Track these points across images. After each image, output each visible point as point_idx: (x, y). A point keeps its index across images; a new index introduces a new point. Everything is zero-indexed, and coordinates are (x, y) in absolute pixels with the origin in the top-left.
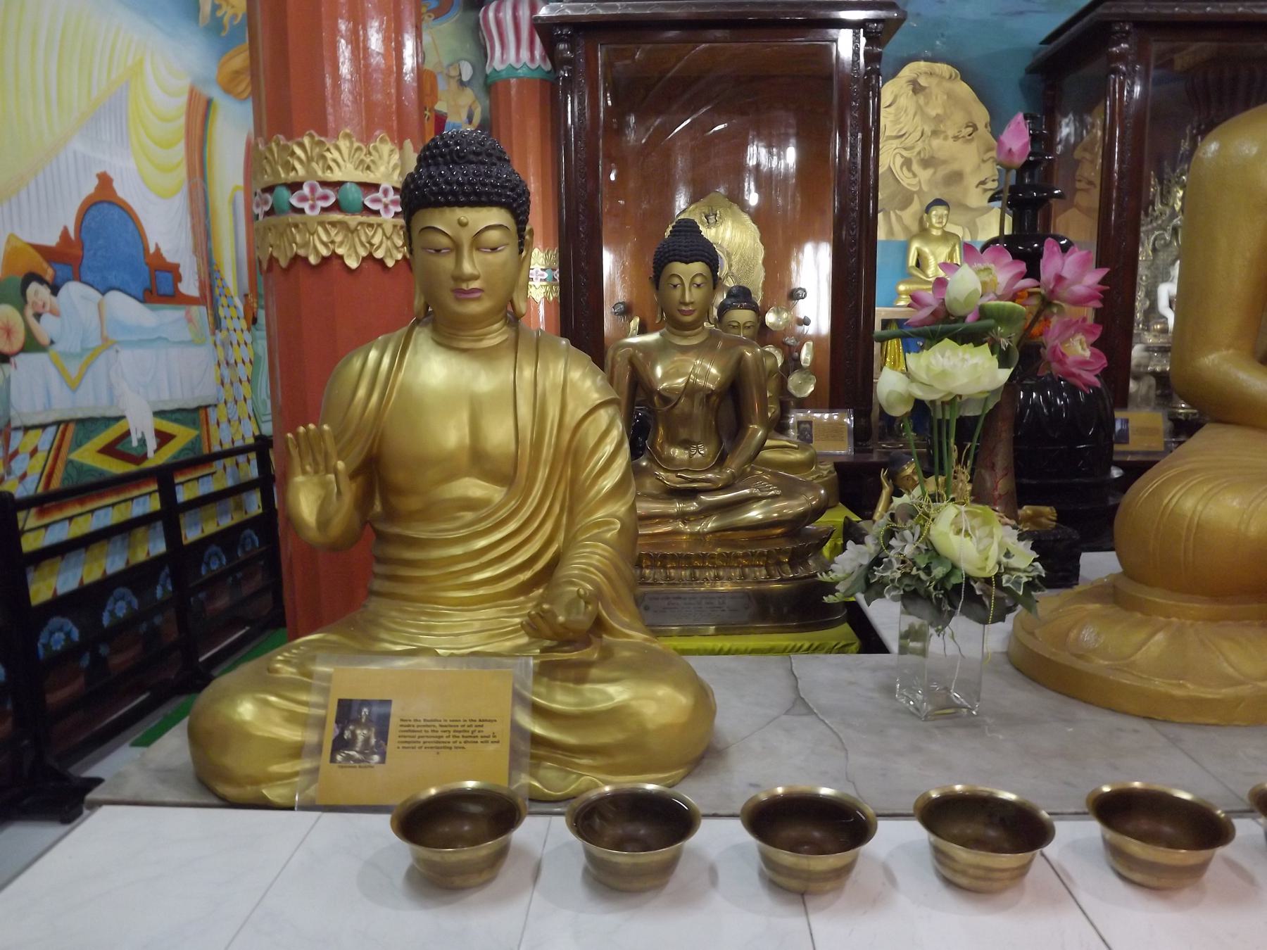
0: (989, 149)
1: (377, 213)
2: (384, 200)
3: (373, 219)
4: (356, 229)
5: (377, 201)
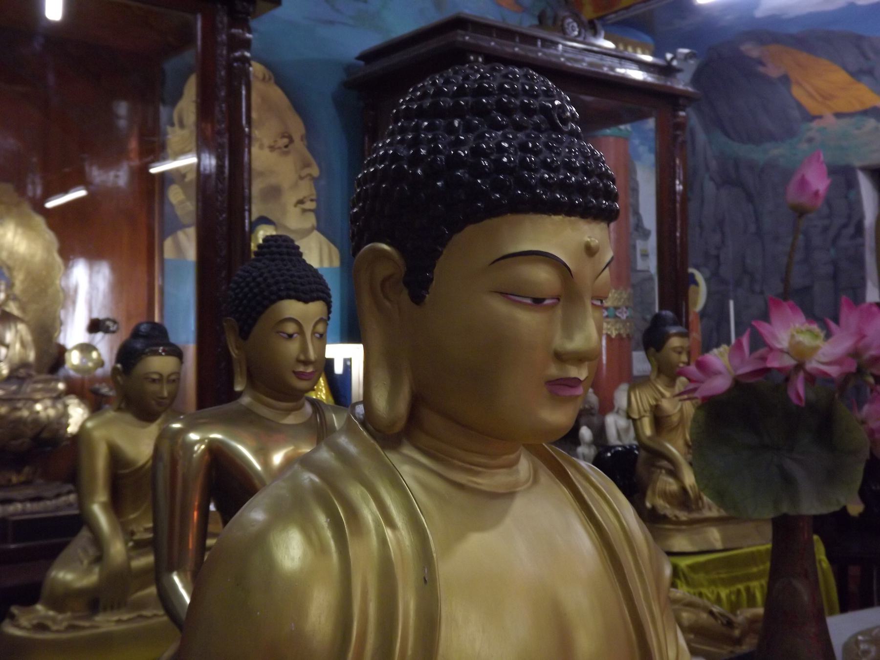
0: (307, 165)
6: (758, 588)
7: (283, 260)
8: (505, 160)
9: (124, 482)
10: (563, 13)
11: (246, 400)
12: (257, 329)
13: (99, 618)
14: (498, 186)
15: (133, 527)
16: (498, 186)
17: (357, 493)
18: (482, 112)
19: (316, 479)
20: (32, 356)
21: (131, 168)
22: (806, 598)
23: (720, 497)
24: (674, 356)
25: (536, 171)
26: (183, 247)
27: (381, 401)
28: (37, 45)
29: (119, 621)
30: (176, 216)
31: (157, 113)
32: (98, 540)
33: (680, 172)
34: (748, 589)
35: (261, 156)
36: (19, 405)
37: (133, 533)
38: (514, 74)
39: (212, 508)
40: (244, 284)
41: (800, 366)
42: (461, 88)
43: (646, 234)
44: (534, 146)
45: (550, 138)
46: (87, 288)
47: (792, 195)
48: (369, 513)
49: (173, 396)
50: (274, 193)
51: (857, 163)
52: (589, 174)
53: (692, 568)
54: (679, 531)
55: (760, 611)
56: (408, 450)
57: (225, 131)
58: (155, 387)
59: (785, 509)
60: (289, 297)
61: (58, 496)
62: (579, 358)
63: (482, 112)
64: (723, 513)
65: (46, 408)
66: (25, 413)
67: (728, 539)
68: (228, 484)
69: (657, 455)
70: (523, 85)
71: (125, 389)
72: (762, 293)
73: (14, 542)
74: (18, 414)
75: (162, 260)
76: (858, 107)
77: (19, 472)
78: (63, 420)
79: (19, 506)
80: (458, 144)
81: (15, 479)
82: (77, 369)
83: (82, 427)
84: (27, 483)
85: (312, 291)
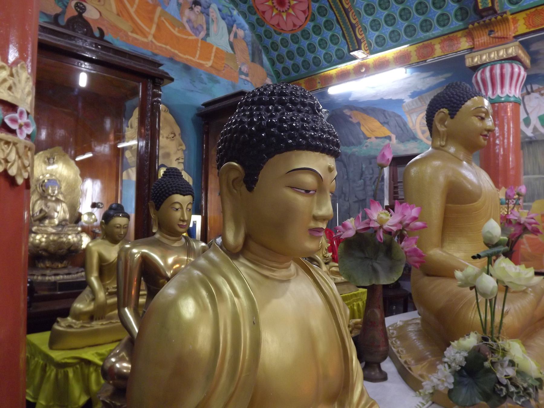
0: (181, 145)
1: (13, 132)
2: (20, 121)
5: (14, 121)
7: (175, 178)
8: (294, 124)
9: (105, 269)
11: (157, 236)
12: (163, 206)
13: (94, 323)
15: (108, 287)
17: (220, 280)
18: (283, 103)
19: (200, 274)
20: (68, 217)
25: (309, 131)
26: (130, 175)
29: (102, 324)
30: (128, 163)
31: (122, 123)
36: (62, 236)
37: (108, 289)
40: (155, 190)
41: (381, 227)
46: (92, 190)
48: (227, 290)
49: (125, 234)
50: (167, 155)
56: (242, 260)
57: (150, 131)
58: (118, 230)
59: (374, 282)
60: (177, 193)
61: (77, 273)
62: (323, 219)
63: (283, 103)
65: (73, 238)
66: (64, 239)
71: (106, 231)
72: (348, 201)
73: (59, 291)
75: (122, 180)
76: (383, 136)
77: (61, 263)
78: (80, 243)
79: (61, 277)
80: (272, 116)
81: (60, 266)
82: (86, 222)
83: (88, 246)
84: (65, 267)
85: (186, 191)
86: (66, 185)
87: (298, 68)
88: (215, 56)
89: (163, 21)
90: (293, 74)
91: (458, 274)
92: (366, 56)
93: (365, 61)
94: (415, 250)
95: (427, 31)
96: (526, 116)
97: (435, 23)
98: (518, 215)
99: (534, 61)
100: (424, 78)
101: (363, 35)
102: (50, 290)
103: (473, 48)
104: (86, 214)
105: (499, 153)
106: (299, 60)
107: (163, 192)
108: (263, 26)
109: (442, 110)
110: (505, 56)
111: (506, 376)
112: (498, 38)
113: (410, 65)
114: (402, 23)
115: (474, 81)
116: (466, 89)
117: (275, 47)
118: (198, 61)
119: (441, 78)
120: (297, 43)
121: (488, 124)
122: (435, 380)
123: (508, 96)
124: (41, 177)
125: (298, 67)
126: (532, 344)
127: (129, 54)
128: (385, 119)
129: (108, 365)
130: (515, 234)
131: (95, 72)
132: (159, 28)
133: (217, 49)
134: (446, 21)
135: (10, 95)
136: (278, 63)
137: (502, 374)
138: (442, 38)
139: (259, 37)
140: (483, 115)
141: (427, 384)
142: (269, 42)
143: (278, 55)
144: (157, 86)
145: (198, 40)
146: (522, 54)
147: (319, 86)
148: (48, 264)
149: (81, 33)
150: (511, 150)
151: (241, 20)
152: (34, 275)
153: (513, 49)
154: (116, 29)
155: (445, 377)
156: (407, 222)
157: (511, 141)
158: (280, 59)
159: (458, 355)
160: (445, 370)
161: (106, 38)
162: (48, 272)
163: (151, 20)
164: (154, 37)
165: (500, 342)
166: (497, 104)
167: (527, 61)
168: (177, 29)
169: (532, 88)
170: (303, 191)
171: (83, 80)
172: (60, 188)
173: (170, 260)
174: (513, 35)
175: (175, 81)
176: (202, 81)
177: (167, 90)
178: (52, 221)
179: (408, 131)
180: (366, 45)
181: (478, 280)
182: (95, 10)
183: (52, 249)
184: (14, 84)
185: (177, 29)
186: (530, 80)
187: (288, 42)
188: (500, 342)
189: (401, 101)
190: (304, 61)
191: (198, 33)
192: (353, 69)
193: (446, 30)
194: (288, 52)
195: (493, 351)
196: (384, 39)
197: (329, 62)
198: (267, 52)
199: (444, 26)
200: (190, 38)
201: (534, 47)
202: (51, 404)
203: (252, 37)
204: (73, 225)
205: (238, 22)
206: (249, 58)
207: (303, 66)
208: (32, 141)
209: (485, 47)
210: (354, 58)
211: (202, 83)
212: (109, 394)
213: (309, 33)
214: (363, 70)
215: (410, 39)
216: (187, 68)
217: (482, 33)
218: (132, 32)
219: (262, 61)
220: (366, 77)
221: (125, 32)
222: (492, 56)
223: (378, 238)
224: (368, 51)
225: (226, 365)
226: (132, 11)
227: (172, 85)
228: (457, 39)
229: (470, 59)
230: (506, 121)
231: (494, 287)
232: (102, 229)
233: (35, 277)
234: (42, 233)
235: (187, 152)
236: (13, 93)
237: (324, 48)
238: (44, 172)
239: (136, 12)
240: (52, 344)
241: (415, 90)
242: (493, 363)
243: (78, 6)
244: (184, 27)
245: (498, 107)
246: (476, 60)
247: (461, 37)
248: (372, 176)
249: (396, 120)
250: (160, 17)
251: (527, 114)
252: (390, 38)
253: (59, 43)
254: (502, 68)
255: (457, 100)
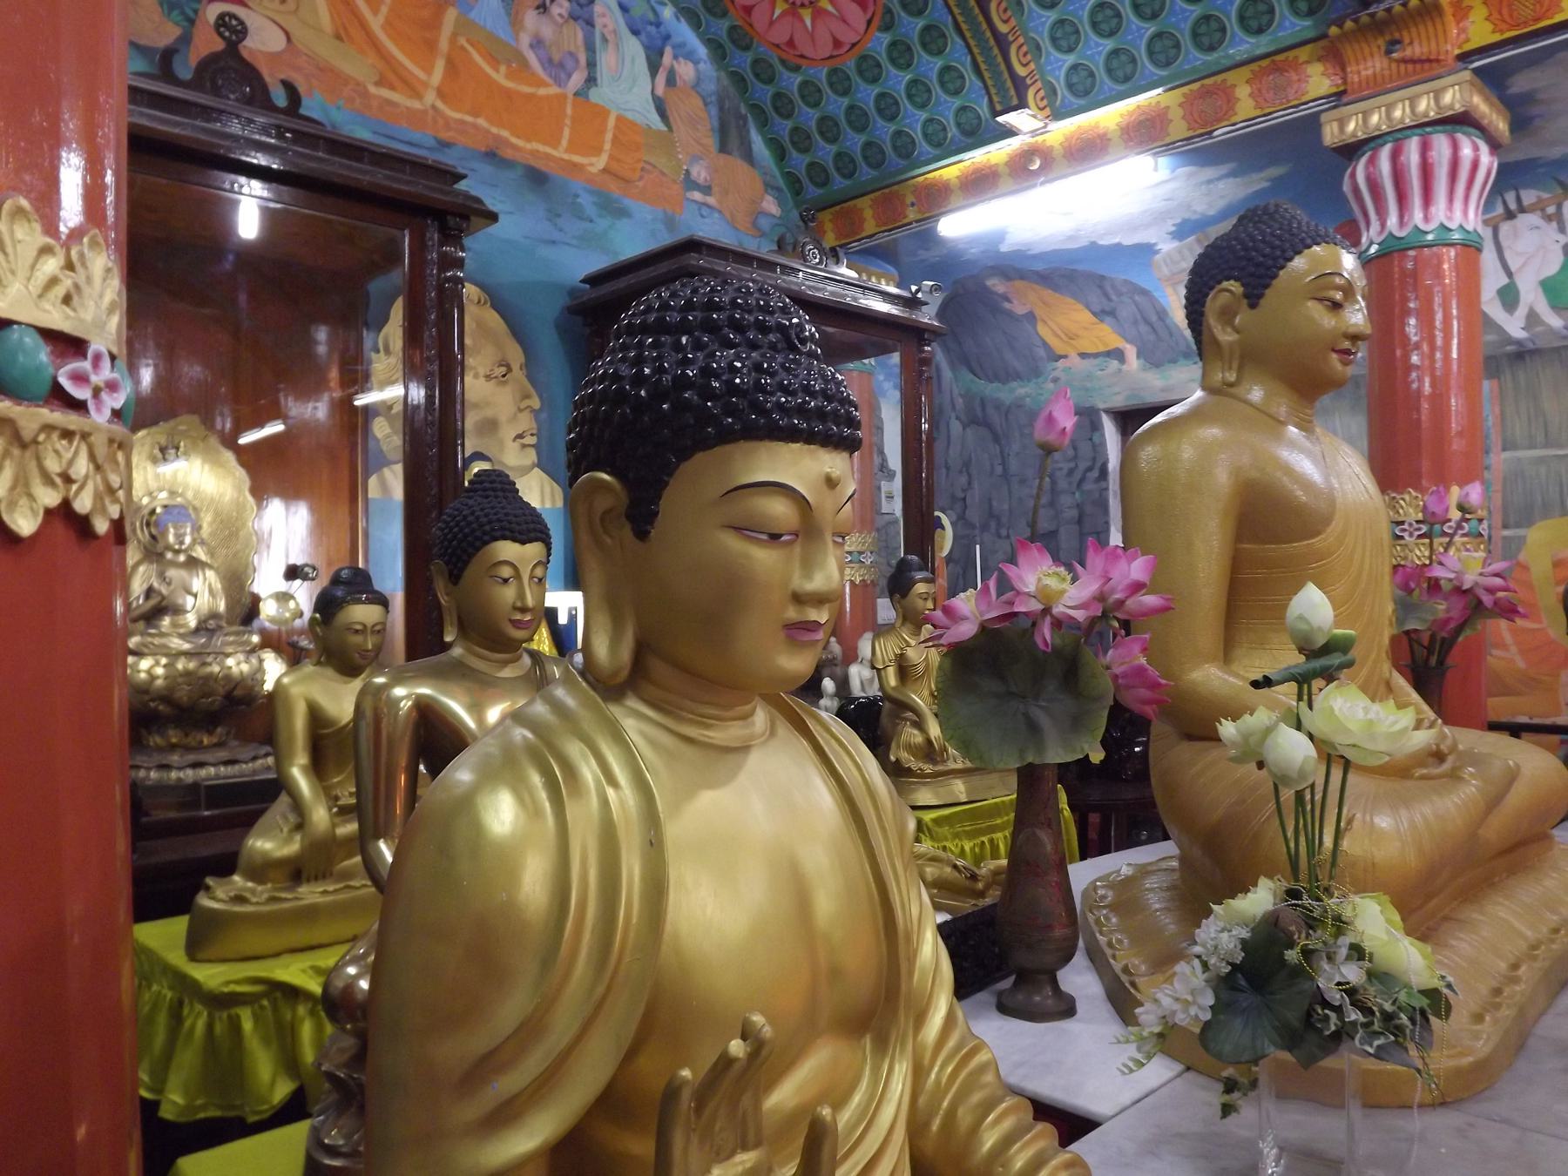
0: (527, 397)
1: (79, 406)
2: (94, 379)
3: (71, 420)
4: (35, 442)
5: (80, 378)
6: (1002, 839)
9: (327, 744)
10: (803, 239)
11: (457, 651)
12: (471, 572)
13: (303, 889)
14: (731, 411)
16: (731, 411)
17: (575, 750)
18: (712, 328)
19: (529, 735)
20: (222, 606)
21: (332, 399)
22: (1049, 848)
23: (966, 748)
24: (920, 603)
25: (772, 394)
26: (388, 486)
27: (601, 649)
28: (228, 263)
29: (325, 892)
31: (360, 341)
32: (298, 806)
33: (925, 410)
34: (991, 841)
35: (475, 386)
36: (209, 659)
37: (337, 798)
38: (748, 288)
39: (422, 767)
40: (456, 519)
41: (1047, 611)
42: (689, 302)
43: (891, 476)
44: (770, 366)
45: (786, 357)
46: (285, 532)
47: (1040, 433)
48: (588, 772)
49: (378, 649)
51: (1101, 406)
52: (829, 399)
53: (936, 821)
54: (925, 784)
55: (1004, 862)
56: (633, 702)
57: (436, 357)
58: (358, 639)
59: (1030, 759)
60: (505, 538)
61: (255, 758)
62: (819, 600)
63: (712, 328)
64: (969, 764)
66: (216, 669)
67: (974, 793)
68: (436, 741)
69: (902, 706)
70: (758, 300)
71: (327, 641)
72: (1008, 537)
74: (208, 669)
75: (366, 499)
76: (1102, 349)
77: (210, 733)
78: (258, 676)
79: (212, 770)
80: (686, 363)
82: (272, 620)
83: (278, 683)
84: (220, 745)
85: (529, 531)
86: (214, 521)
87: (851, 166)
88: (615, 139)
89: (462, 48)
90: (839, 182)
91: (1227, 729)
92: (1041, 124)
93: (1040, 139)
94: (1140, 671)
95: (1212, 48)
96: (1505, 280)
97: (1233, 25)
98: (1458, 567)
99: (1520, 124)
100: (1209, 182)
101: (1032, 66)
102: (182, 806)
103: (1344, 92)
104: (271, 596)
105: (1419, 391)
106: (855, 141)
107: (466, 536)
108: (747, 48)
109: (1225, 284)
110: (1457, 106)
111: (1339, 984)
112: (1413, 61)
113: (1168, 148)
114: (1139, 29)
115: (1346, 187)
116: (1290, 224)
117: (783, 105)
118: (566, 157)
119: (1257, 182)
120: (845, 93)
121: (1353, 320)
122: (1166, 1002)
123: (1443, 227)
124: (145, 501)
125: (853, 161)
126: (1475, 915)
127: (373, 153)
128: (1104, 300)
129: (339, 984)
130: (1447, 621)
131: (279, 206)
132: (452, 68)
133: (620, 119)
134: (1265, 19)
135: (67, 317)
136: (795, 154)
137: (1330, 980)
138: (1254, 66)
139: (739, 80)
140: (1338, 296)
141: (1147, 1013)
142: (765, 93)
143: (795, 130)
144: (452, 236)
145: (564, 97)
146: (1482, 105)
147: (912, 214)
148: (174, 736)
149: (237, 100)
150: (1453, 382)
151: (684, 32)
152: (138, 767)
153: (1455, 94)
154: (332, 77)
155: (1192, 993)
156: (1117, 596)
157: (1455, 355)
158: (801, 140)
159: (1225, 935)
160: (1194, 973)
161: (310, 108)
162: (175, 758)
163: (431, 46)
164: (441, 93)
165: (1332, 903)
166: (1412, 253)
167: (1500, 125)
168: (503, 69)
169: (1519, 200)
170: (764, 537)
171: (248, 222)
172: (197, 528)
173: (493, 714)
174: (1457, 52)
175: (501, 217)
176: (579, 214)
177: (478, 246)
178: (181, 619)
179: (1171, 335)
180: (1042, 93)
181: (1268, 741)
182: (276, 28)
183: (183, 694)
184: (77, 286)
185: (503, 69)
186: (1510, 176)
187: (819, 91)
188: (1332, 903)
189: (1147, 250)
190: (868, 145)
191: (563, 76)
192: (1007, 164)
193: (1262, 44)
194: (823, 120)
195: (1311, 923)
196: (1092, 75)
197: (938, 145)
198: (763, 122)
199: (1260, 31)
200: (542, 91)
201: (1520, 84)
202: (199, 1102)
203: (718, 79)
204: (235, 628)
205: (676, 39)
206: (711, 142)
207: (865, 158)
208: (125, 424)
209: (1376, 89)
210: (1009, 132)
211: (581, 218)
212: (346, 1056)
213: (879, 65)
214: (1036, 165)
215: (1163, 73)
216: (537, 178)
217: (1367, 50)
218: (378, 84)
219: (750, 149)
220: (1042, 184)
221: (358, 84)
222: (1398, 113)
223: (1039, 641)
224: (1048, 111)
225: (587, 936)
226: (376, 23)
227: (494, 229)
228: (1295, 66)
229: (1335, 125)
230: (1437, 300)
231: (1306, 758)
232: (315, 638)
233: (142, 773)
234: (154, 654)
235: (544, 416)
236: (74, 310)
237: (923, 106)
238: (153, 485)
239: (388, 25)
240: (195, 947)
241: (1187, 216)
242: (1307, 953)
243: (225, 25)
244: (524, 64)
245: (1415, 258)
246: (1351, 126)
247: (1308, 62)
248: (1072, 465)
249: (1135, 302)
250: (454, 36)
251: (1509, 274)
252: (1109, 71)
253: (177, 131)
254: (1425, 148)
255: (1264, 256)
